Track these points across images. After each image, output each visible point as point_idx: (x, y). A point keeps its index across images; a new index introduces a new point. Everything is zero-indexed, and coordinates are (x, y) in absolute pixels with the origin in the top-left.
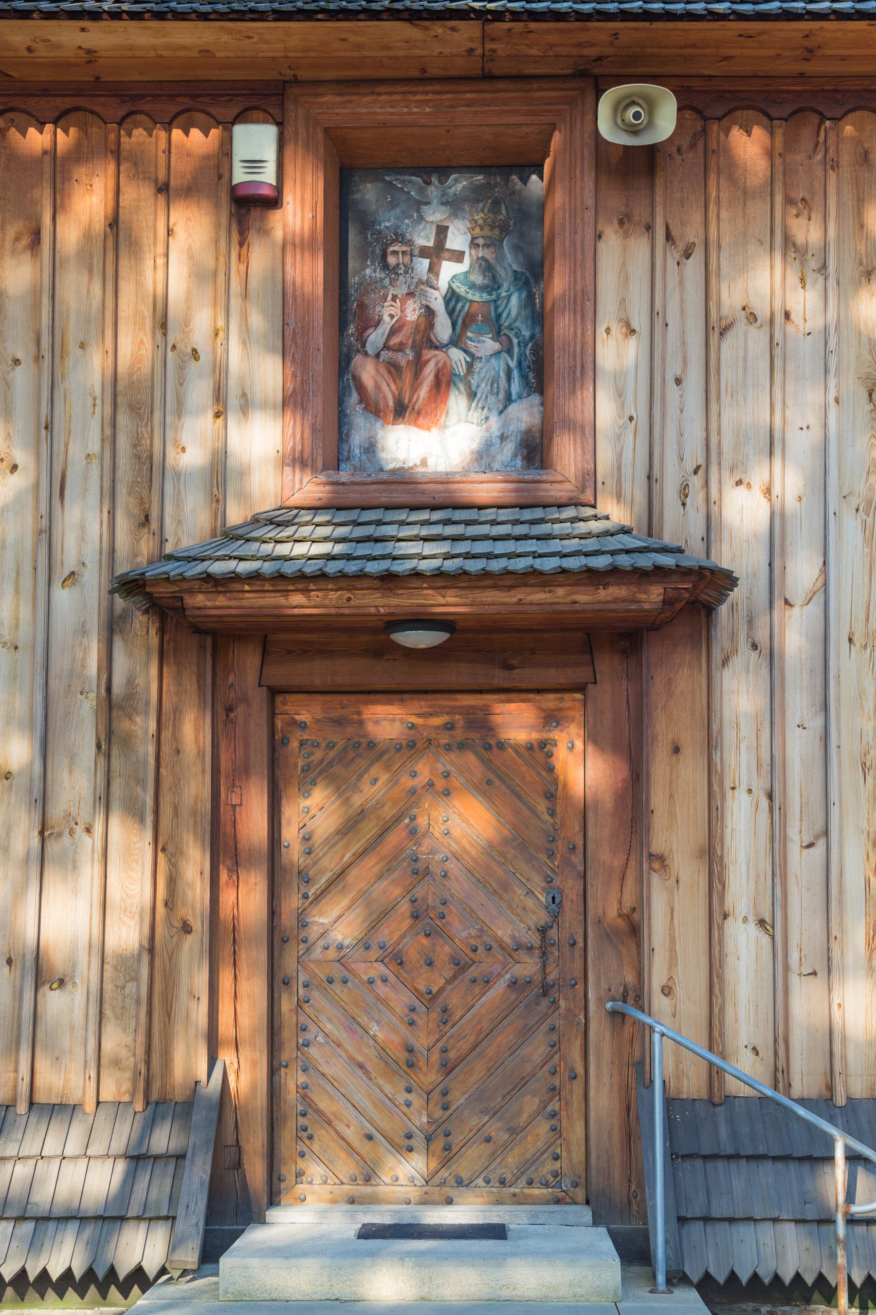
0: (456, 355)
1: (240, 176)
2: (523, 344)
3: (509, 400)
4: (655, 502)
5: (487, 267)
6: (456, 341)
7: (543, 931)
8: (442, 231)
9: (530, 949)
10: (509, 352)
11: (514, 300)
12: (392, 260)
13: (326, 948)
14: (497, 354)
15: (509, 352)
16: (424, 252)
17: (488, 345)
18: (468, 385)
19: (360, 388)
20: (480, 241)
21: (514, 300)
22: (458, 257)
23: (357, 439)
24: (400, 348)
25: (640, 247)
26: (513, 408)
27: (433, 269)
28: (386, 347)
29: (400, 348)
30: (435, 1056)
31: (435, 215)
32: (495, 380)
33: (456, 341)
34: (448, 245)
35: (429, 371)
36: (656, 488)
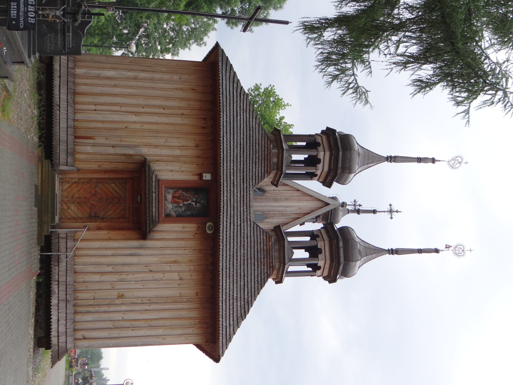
2: (184, 214)
3: (175, 212)
4: (105, 274)
6: (184, 204)
7: (98, 216)
8: (199, 203)
9: (96, 215)
10: (182, 212)
11: (189, 213)
12: (195, 196)
13: (90, 183)
14: (182, 210)
15: (182, 212)
16: (196, 200)
17: (183, 209)
18: (177, 206)
19: (177, 191)
20: (435, 62)
21: (189, 213)
22: (196, 205)
23: (170, 190)
24: (183, 197)
25: (195, 229)
26: (174, 213)
27: (194, 202)
28: (183, 195)
29: (183, 197)
30: (80, 201)
31: (202, 201)
32: (178, 210)
33: (184, 204)
34: (197, 204)
35: (180, 201)
36: (110, 274)
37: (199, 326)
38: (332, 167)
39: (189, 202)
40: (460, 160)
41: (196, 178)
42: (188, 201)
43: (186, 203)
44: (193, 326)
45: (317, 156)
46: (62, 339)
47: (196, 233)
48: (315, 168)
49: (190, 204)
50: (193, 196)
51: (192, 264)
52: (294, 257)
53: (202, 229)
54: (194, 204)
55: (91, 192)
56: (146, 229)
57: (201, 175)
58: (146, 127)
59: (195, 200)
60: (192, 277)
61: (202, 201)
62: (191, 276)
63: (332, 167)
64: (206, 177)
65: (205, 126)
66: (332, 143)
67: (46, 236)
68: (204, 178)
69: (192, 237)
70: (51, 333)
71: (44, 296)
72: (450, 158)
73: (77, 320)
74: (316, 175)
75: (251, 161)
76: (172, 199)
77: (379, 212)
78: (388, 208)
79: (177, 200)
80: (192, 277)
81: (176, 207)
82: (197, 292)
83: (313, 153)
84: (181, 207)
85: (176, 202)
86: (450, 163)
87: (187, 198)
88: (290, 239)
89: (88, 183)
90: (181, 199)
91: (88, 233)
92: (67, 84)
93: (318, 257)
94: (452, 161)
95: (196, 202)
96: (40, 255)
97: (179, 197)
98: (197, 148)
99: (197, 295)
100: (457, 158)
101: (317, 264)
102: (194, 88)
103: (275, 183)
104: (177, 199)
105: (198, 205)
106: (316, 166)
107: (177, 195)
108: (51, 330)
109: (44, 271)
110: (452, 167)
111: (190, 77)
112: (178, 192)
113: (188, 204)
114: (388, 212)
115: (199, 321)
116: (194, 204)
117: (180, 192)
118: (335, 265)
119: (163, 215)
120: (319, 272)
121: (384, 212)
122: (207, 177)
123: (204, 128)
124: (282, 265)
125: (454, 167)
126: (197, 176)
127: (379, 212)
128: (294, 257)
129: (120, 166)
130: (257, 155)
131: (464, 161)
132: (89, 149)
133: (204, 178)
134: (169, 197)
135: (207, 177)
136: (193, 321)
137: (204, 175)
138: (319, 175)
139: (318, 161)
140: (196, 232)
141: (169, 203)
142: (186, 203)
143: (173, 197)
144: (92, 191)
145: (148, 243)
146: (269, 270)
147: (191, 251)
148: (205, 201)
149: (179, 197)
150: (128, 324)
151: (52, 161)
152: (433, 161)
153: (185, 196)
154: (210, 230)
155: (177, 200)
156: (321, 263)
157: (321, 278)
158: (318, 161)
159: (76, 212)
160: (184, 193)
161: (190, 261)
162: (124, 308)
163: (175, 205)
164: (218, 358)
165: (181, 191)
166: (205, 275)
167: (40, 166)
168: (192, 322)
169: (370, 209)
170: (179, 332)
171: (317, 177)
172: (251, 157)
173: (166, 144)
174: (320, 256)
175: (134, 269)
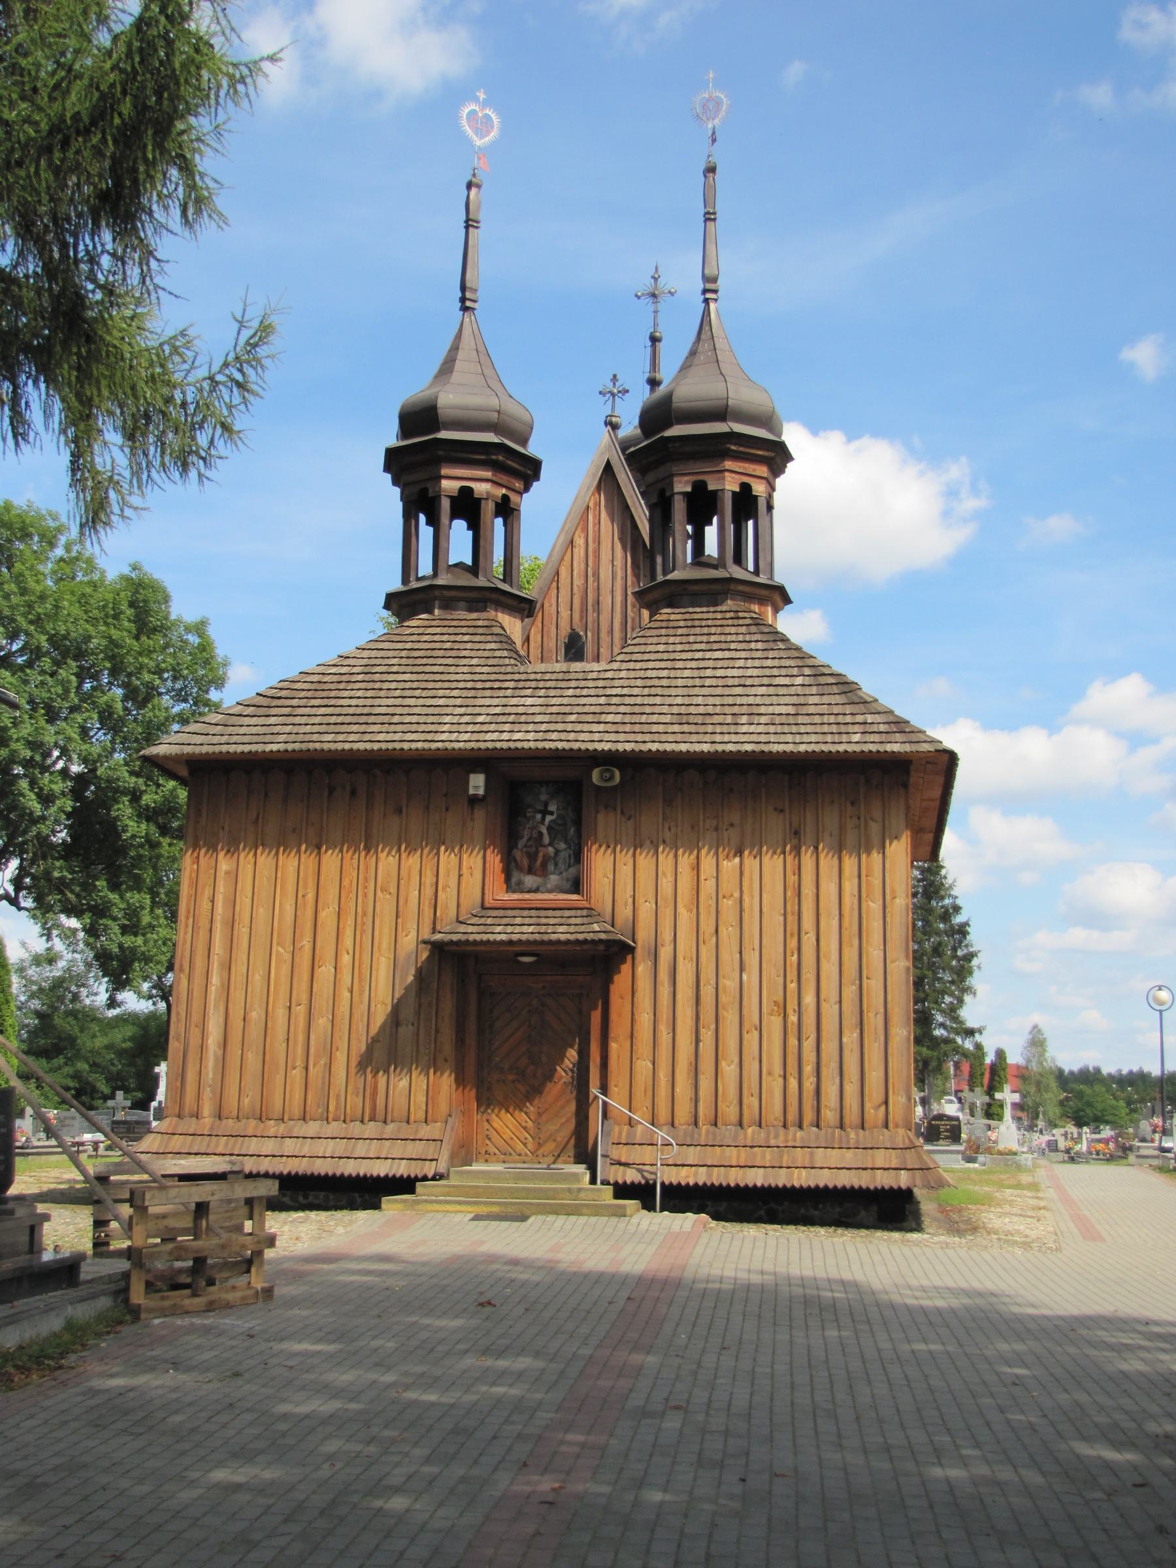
0: (551, 850)
1: (471, 792)
3: (570, 866)
5: (559, 816)
6: (551, 844)
8: (546, 804)
16: (540, 812)
17: (562, 846)
19: (515, 860)
22: (552, 813)
24: (531, 846)
27: (543, 819)
29: (531, 846)
31: (543, 797)
33: (551, 844)
35: (541, 855)
37: (862, 806)
39: (545, 831)
41: (480, 814)
42: (541, 834)
43: (546, 840)
44: (862, 819)
45: (451, 498)
46: (880, 1158)
47: (622, 813)
48: (483, 502)
49: (549, 829)
50: (528, 819)
51: (701, 823)
52: (715, 554)
53: (607, 797)
54: (549, 818)
55: (513, 1082)
56: (601, 941)
57: (474, 800)
58: (348, 941)
59: (539, 816)
60: (737, 821)
61: (543, 797)
62: (732, 825)
64: (476, 787)
65: (348, 788)
66: (483, 457)
67: (617, 1195)
68: (481, 792)
69: (630, 824)
70: (780, 1185)
71: (773, 1205)
73: (277, 1115)
74: (505, 498)
75: (452, 669)
76: (535, 874)
77: (655, 325)
78: (647, 305)
79: (539, 862)
80: (737, 821)
81: (556, 864)
82: (776, 809)
83: (446, 504)
84: (557, 852)
85: (544, 865)
87: (535, 835)
88: (425, 566)
89: (489, 1089)
91: (613, 1089)
93: (715, 492)
95: (545, 812)
96: (661, 1211)
97: (532, 857)
98: (404, 811)
99: (782, 811)
101: (734, 493)
102: (255, 816)
103: (526, 606)
104: (536, 861)
106: (479, 500)
107: (525, 862)
108: (856, 1187)
109: (710, 1203)
111: (227, 828)
112: (518, 858)
113: (549, 834)
115: (849, 807)
116: (549, 818)
117: (517, 854)
119: (575, 897)
120: (759, 489)
122: (477, 783)
123: (353, 793)
124: (732, 587)
126: (476, 811)
127: (655, 325)
128: (715, 554)
129: (448, 1006)
130: (441, 653)
133: (481, 792)
135: (477, 783)
136: (848, 820)
137: (471, 792)
138: (504, 491)
139: (466, 492)
140: (619, 811)
141: (545, 884)
142: (546, 840)
143: (530, 871)
144: (510, 1077)
145: (644, 936)
146: (741, 622)
147: (666, 826)
148: (543, 789)
149: (532, 857)
151: (417, 1179)
153: (529, 840)
154: (612, 777)
155: (539, 862)
156: (731, 485)
157: (778, 481)
158: (466, 492)
159: (563, 1120)
160: (521, 844)
161: (693, 827)
162: (809, 999)
163: (551, 867)
164: (946, 757)
165: (515, 851)
166: (731, 790)
167: (429, 1207)
168: (850, 824)
169: (649, 350)
171: (513, 497)
172: (441, 669)
173: (393, 890)
174: (711, 487)
175: (708, 973)
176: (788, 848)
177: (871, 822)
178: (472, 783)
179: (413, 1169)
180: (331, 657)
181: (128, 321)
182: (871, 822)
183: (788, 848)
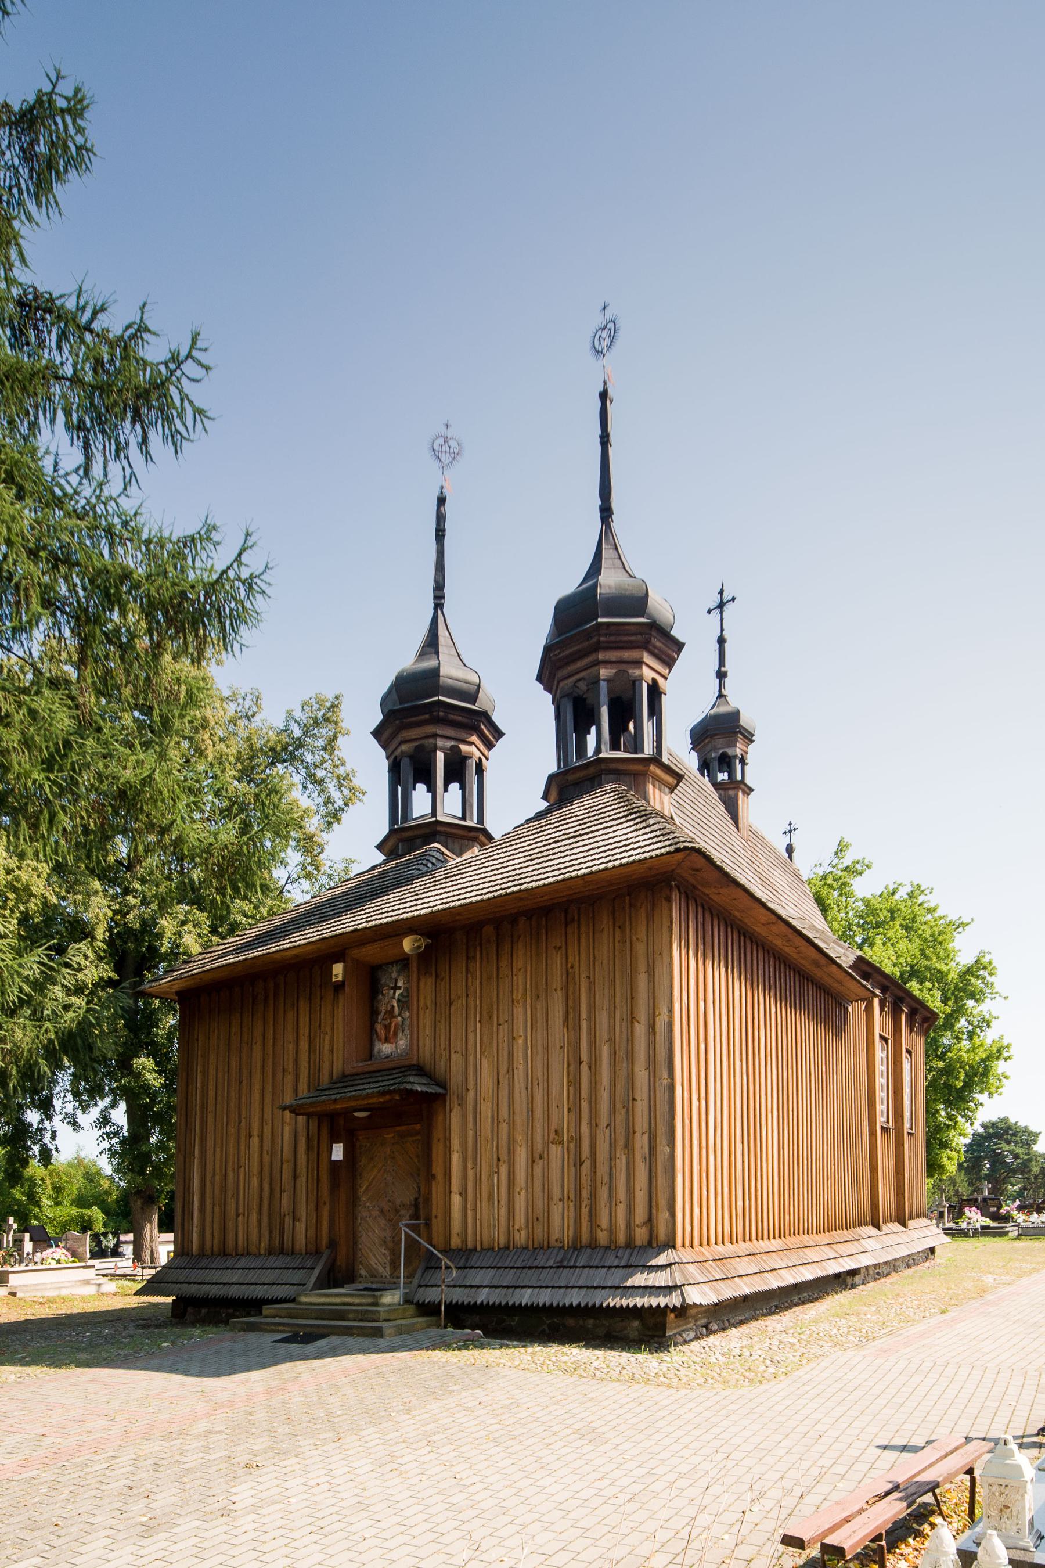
0: (399, 1019)
6: (400, 1015)
16: (392, 988)
19: (377, 1033)
22: (400, 988)
31: (394, 975)
33: (400, 1015)
35: (393, 1025)
38: (427, 716)
39: (395, 1005)
40: (441, 441)
42: (393, 1007)
43: (396, 1010)
49: (399, 1001)
54: (398, 992)
57: (339, 987)
63: (427, 716)
64: (337, 975)
72: (436, 464)
77: (722, 630)
85: (395, 1034)
86: (448, 461)
90: (390, 1024)
92: (563, 1290)
94: (443, 459)
95: (396, 988)
97: (387, 1028)
100: (436, 447)
105: (400, 983)
110: (455, 456)
114: (721, 613)
116: (398, 992)
118: (606, 635)
121: (722, 620)
125: (456, 451)
131: (443, 430)
132: (301, 1227)
134: (386, 1048)
142: (396, 1010)
143: (387, 1040)
148: (394, 969)
149: (387, 1028)
150: (620, 1118)
152: (441, 501)
160: (380, 1017)
163: (400, 1035)
170: (642, 980)
176: (915, 1526)
177: (636, 1024)
178: (334, 973)
179: (259, 1292)
180: (1022, 1124)
181: (216, 739)
182: (636, 1024)
183: (915, 1526)
